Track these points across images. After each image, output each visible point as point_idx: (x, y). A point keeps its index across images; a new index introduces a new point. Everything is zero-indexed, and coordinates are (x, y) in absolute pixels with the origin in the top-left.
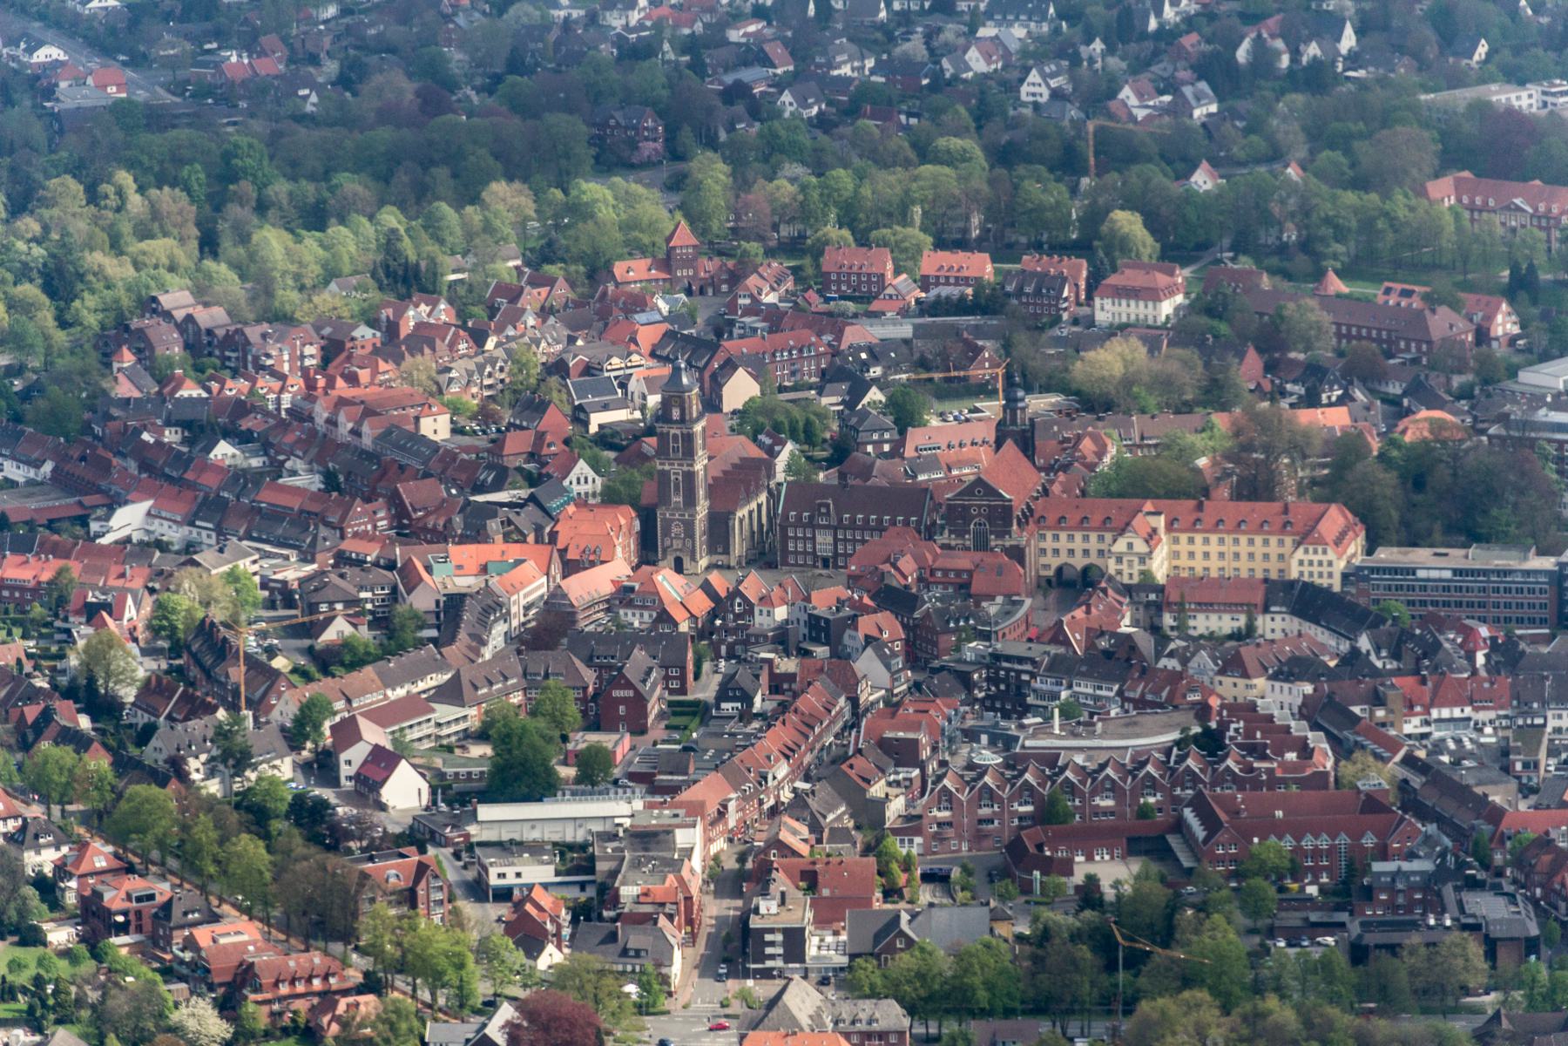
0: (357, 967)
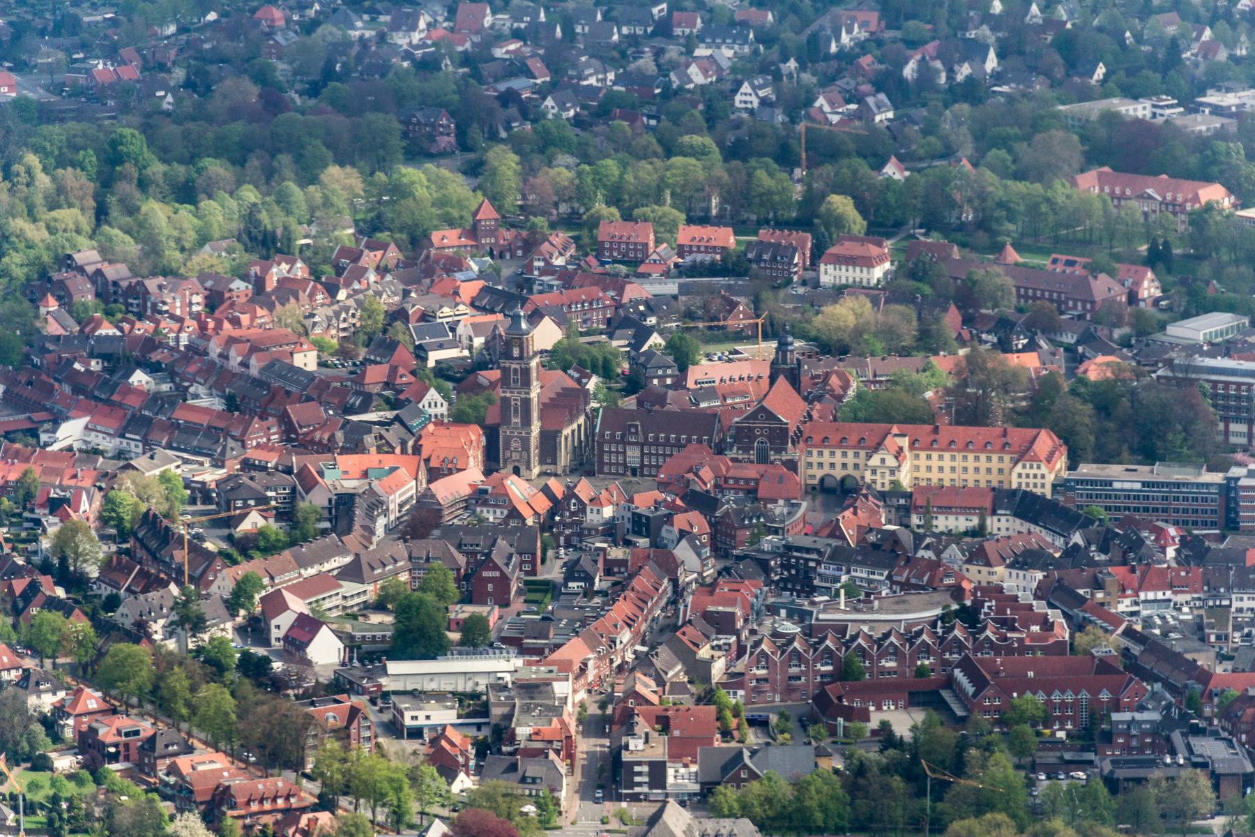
0: (310, 791)
